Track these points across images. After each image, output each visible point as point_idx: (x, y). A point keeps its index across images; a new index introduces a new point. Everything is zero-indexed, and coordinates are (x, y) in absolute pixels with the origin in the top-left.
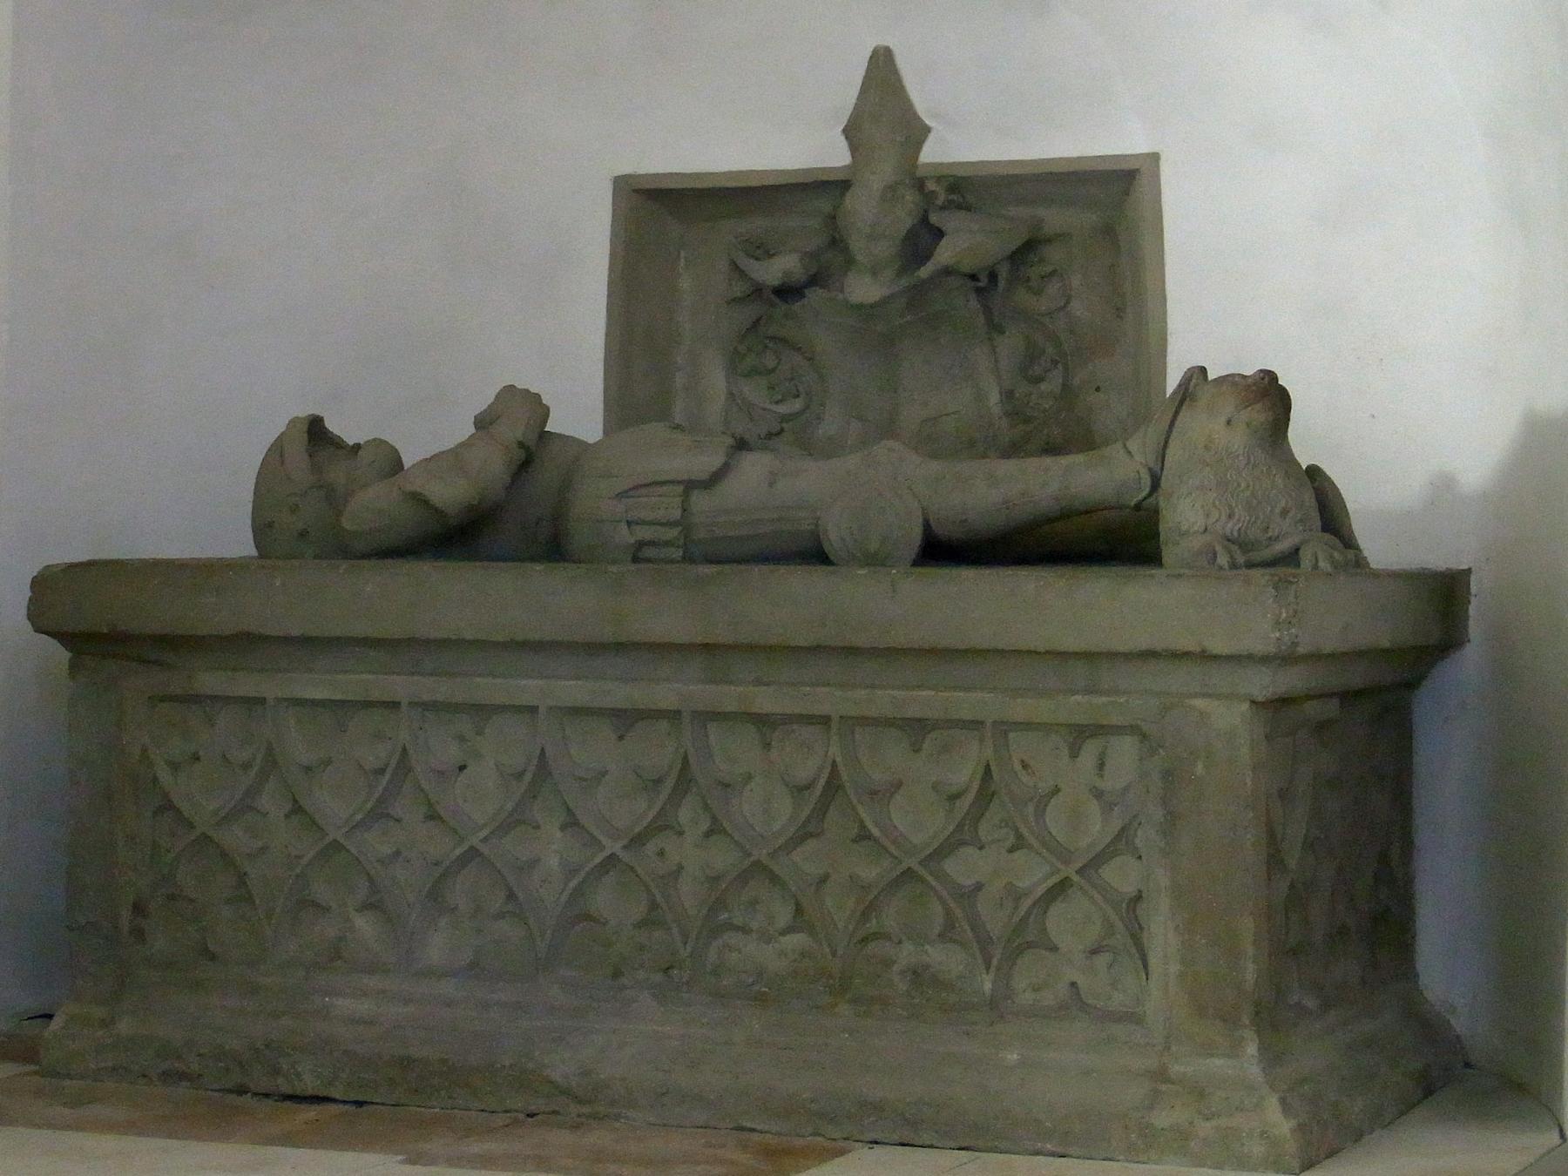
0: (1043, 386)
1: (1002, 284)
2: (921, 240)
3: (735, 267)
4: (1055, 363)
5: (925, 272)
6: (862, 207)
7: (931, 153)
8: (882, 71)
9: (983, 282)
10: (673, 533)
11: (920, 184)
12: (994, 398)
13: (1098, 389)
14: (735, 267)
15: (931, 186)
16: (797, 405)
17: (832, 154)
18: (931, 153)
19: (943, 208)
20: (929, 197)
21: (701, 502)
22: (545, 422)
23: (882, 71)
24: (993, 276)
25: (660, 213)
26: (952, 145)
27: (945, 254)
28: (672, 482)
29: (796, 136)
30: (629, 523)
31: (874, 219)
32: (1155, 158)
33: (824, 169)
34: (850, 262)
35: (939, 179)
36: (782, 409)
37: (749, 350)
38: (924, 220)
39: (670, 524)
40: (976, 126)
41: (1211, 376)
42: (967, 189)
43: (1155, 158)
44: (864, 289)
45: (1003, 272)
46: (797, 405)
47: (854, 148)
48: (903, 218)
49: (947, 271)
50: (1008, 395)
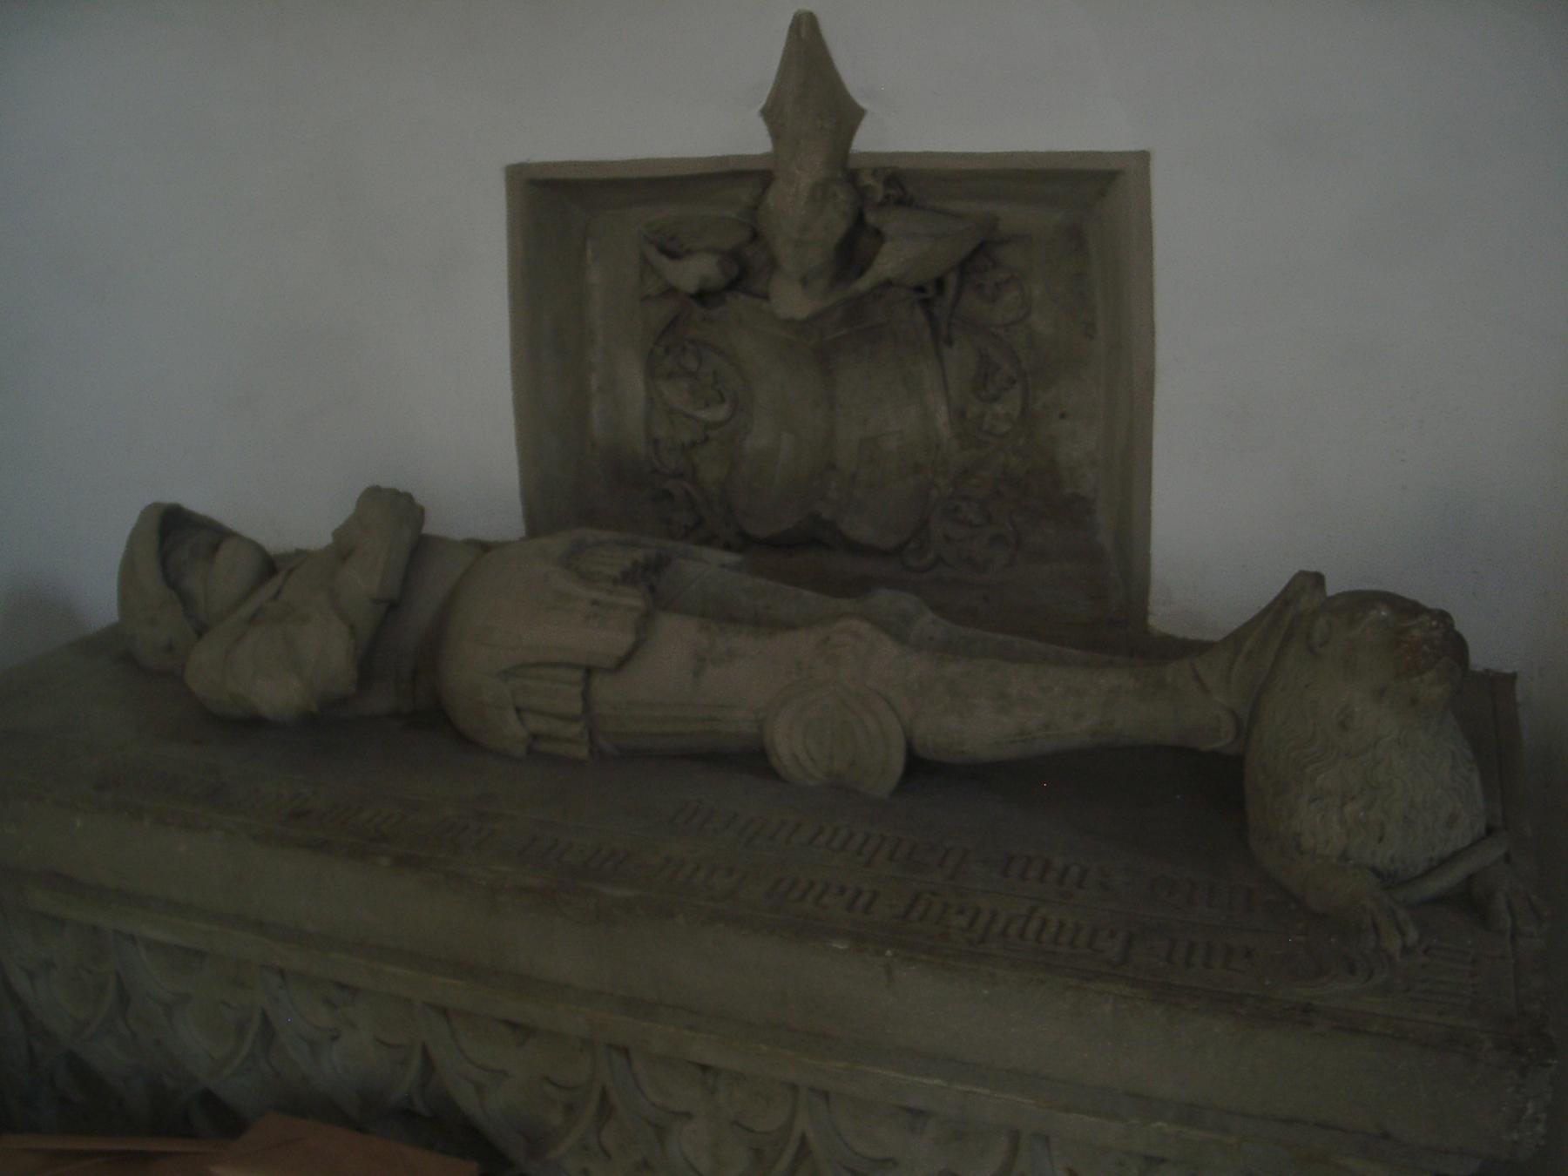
0: (998, 408)
1: (950, 291)
2: (853, 252)
3: (645, 260)
4: (1012, 382)
5: (864, 284)
6: (789, 203)
7: (867, 141)
8: (807, 47)
9: (928, 293)
10: (576, 729)
11: (852, 177)
12: (942, 417)
13: (1063, 416)
14: (645, 260)
15: (867, 180)
16: (720, 413)
17: (751, 139)
18: (867, 141)
19: (882, 205)
20: (861, 194)
21: (606, 690)
22: (420, 528)
23: (807, 47)
24: (940, 284)
25: (559, 210)
26: (893, 130)
27: (889, 262)
28: (569, 665)
29: (716, 120)
30: (518, 710)
31: (801, 220)
32: (1144, 157)
33: (739, 157)
34: (773, 264)
35: (875, 173)
36: (705, 415)
37: (667, 350)
38: (859, 219)
39: (574, 719)
40: (913, 113)
41: (1332, 589)
42: (906, 185)
43: (1144, 157)
44: (792, 300)
45: (952, 280)
46: (720, 413)
47: (776, 136)
48: (835, 222)
49: (888, 283)
50: (959, 414)
